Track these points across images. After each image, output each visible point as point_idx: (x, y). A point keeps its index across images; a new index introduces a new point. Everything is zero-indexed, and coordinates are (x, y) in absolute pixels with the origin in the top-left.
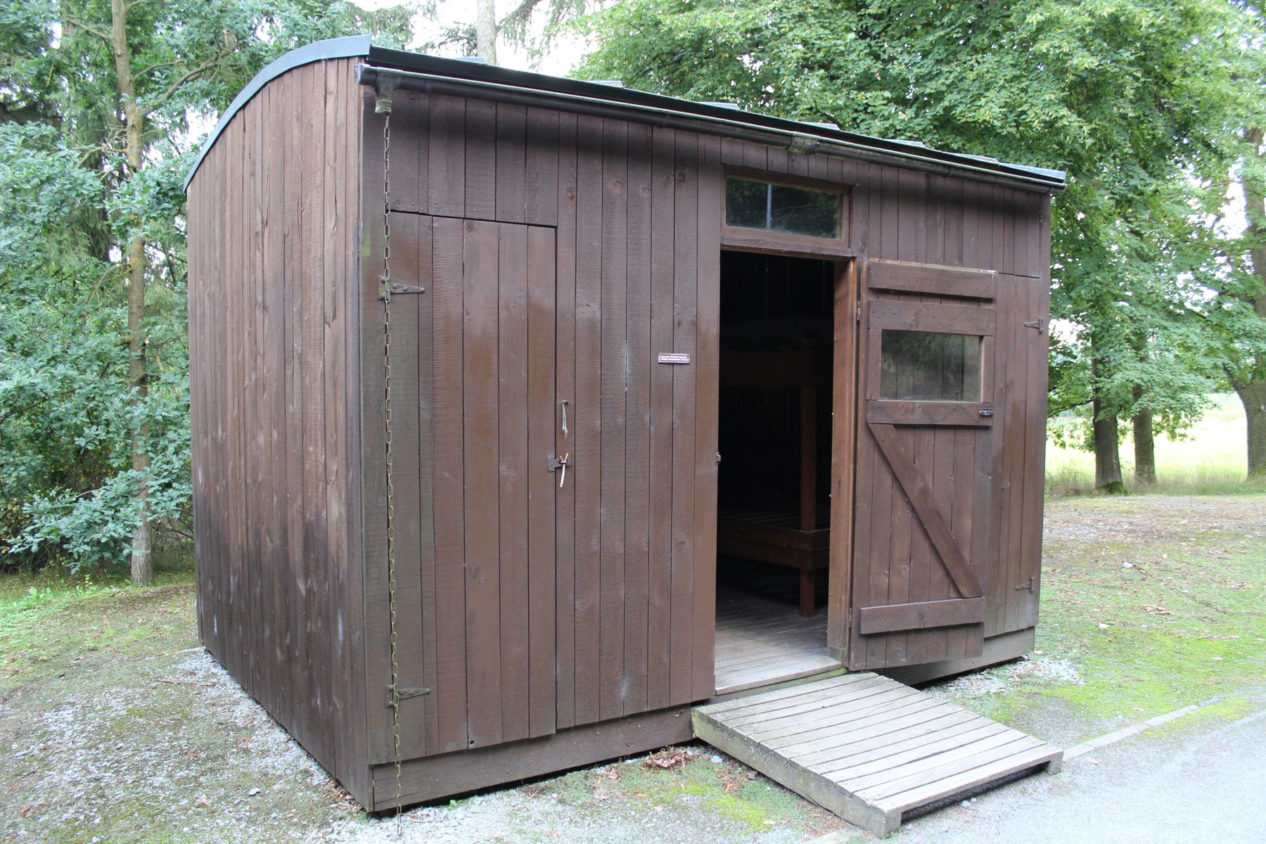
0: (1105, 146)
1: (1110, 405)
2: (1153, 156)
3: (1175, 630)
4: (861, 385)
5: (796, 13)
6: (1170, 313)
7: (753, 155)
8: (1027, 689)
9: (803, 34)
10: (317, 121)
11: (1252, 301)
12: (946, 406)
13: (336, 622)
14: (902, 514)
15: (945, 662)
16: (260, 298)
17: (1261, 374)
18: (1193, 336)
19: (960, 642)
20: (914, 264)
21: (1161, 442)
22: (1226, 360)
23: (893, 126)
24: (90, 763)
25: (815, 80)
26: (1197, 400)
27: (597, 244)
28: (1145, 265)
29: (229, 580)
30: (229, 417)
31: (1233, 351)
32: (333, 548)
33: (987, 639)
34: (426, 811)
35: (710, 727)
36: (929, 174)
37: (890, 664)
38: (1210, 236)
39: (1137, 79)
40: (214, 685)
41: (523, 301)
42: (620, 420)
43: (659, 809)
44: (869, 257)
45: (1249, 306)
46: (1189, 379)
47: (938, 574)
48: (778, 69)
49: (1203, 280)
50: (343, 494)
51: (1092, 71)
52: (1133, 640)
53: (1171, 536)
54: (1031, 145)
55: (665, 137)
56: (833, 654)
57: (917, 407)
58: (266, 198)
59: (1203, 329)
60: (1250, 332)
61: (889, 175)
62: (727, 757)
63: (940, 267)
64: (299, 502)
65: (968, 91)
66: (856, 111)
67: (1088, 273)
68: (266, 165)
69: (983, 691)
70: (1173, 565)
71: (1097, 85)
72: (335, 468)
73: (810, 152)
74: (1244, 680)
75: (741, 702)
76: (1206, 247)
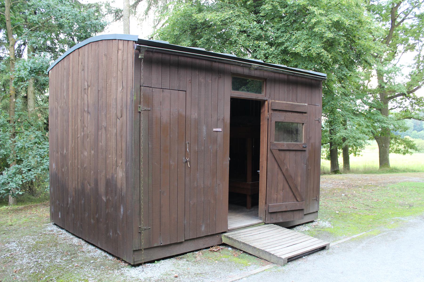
0: (335, 61)
1: (335, 144)
2: (350, 65)
3: (358, 213)
4: (269, 138)
5: (237, 14)
6: (354, 113)
7: (240, 70)
8: (317, 229)
9: (240, 22)
10: (114, 58)
11: (380, 110)
12: (293, 144)
13: (120, 208)
14: (281, 176)
15: (293, 221)
16: (86, 109)
17: (383, 134)
18: (362, 121)
19: (298, 215)
20: (284, 102)
21: (351, 156)
22: (372, 129)
23: (268, 53)
24: (31, 258)
25: (243, 37)
26: (363, 142)
27: (197, 96)
28: (346, 98)
29: (68, 199)
30: (70, 147)
31: (374, 126)
32: (119, 186)
33: (305, 215)
34: (148, 264)
35: (228, 239)
36: (288, 75)
37: (277, 222)
38: (367, 87)
39: (345, 41)
40: (62, 234)
41: (177, 113)
42: (203, 148)
43: (216, 262)
44: (271, 100)
45: (379, 112)
46: (361, 135)
47: (291, 194)
48: (231, 33)
49: (365, 103)
50: (124, 170)
51: (331, 38)
52: (346, 216)
53: (356, 186)
54: (310, 59)
55: (216, 65)
56: (261, 219)
57: (285, 144)
58: (90, 78)
59: (365, 119)
60: (380, 120)
61: (277, 75)
62: (232, 247)
63: (291, 103)
64: (104, 172)
65: (292, 42)
66: (256, 47)
67: (329, 101)
68: (90, 68)
69: (304, 230)
70: (357, 195)
71: (333, 42)
72: (121, 162)
73: (256, 69)
74: (378, 225)
75: (236, 232)
76: (366, 91)
